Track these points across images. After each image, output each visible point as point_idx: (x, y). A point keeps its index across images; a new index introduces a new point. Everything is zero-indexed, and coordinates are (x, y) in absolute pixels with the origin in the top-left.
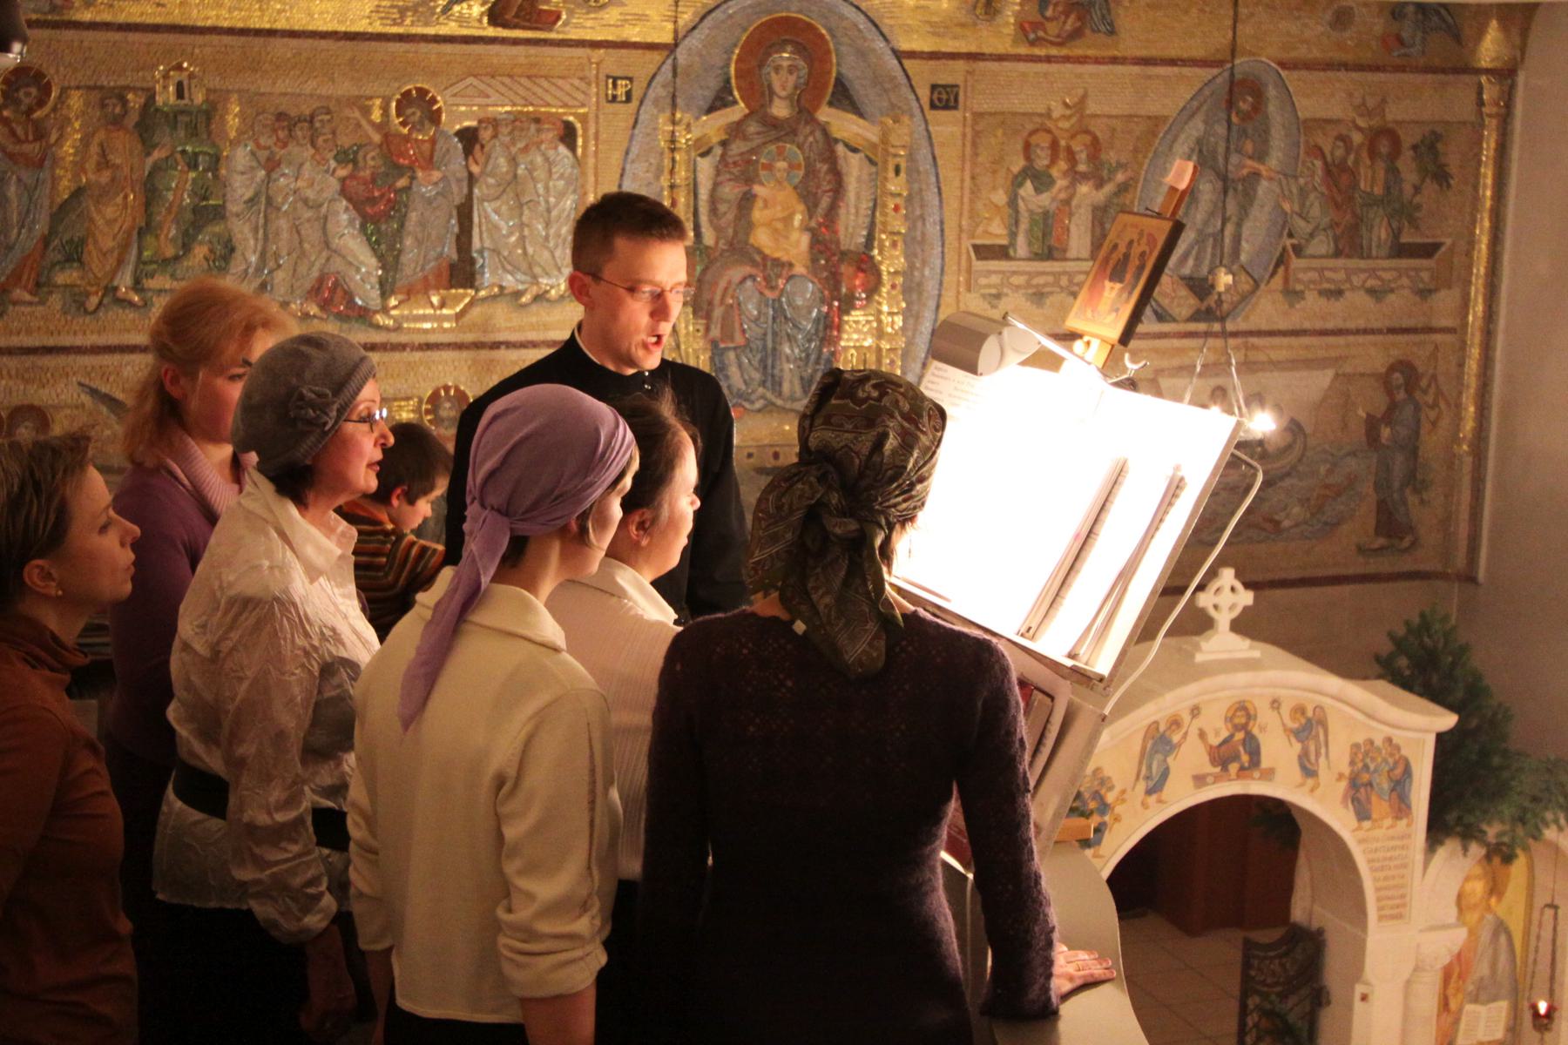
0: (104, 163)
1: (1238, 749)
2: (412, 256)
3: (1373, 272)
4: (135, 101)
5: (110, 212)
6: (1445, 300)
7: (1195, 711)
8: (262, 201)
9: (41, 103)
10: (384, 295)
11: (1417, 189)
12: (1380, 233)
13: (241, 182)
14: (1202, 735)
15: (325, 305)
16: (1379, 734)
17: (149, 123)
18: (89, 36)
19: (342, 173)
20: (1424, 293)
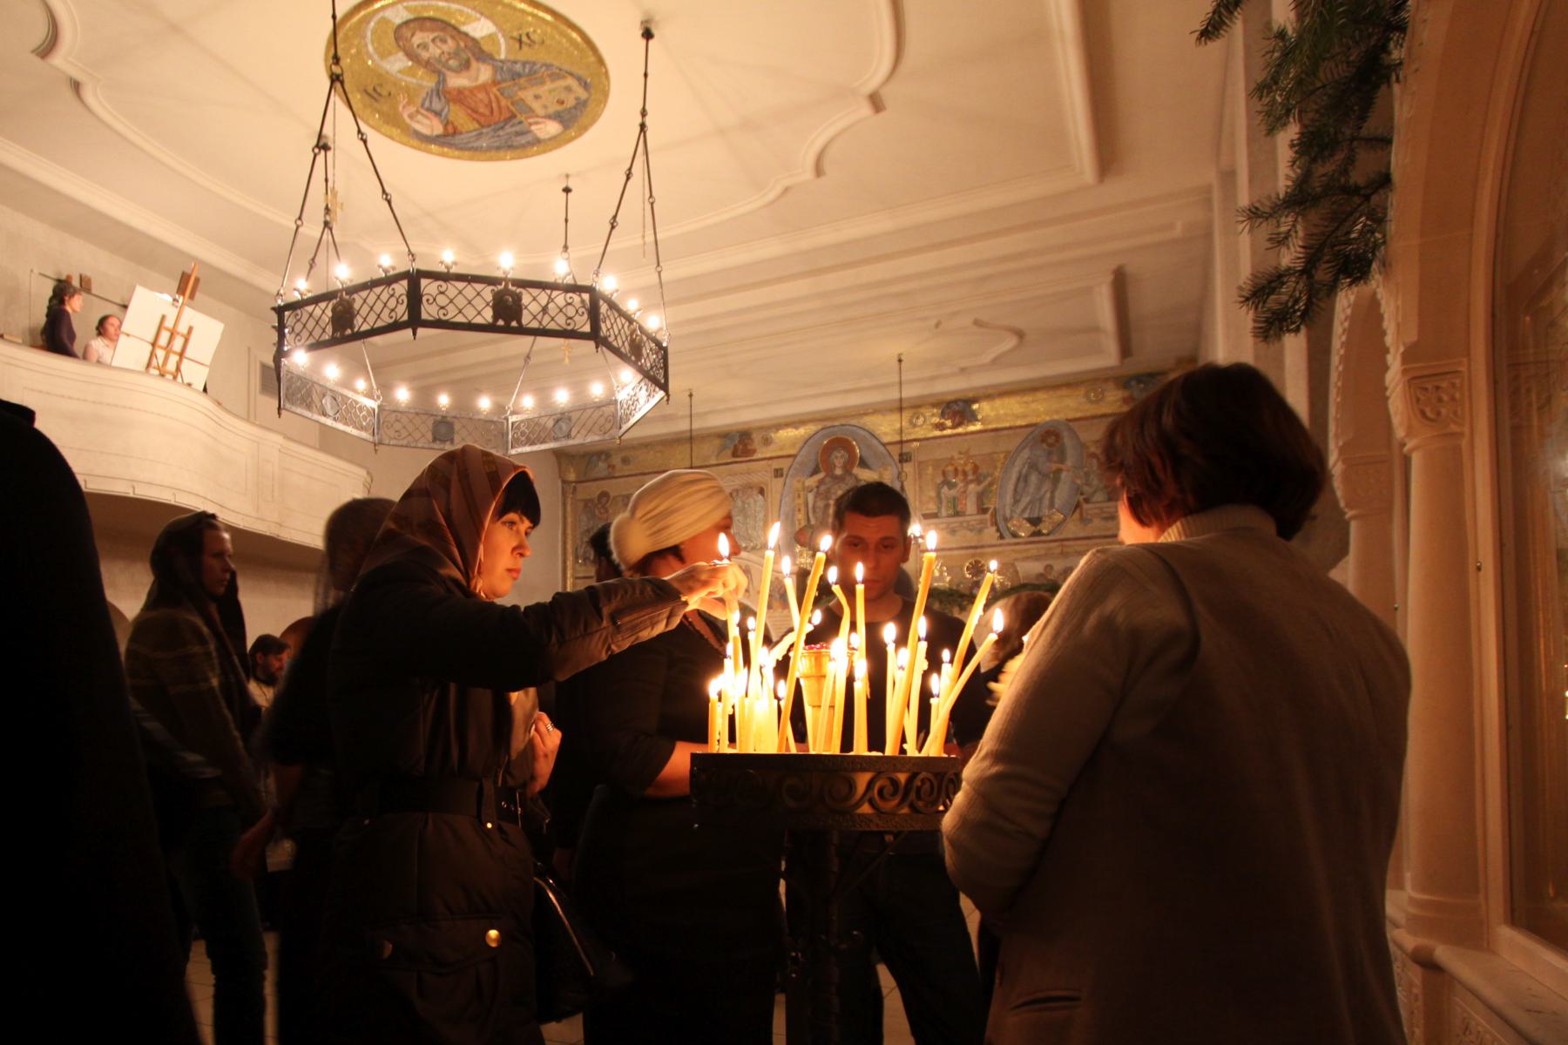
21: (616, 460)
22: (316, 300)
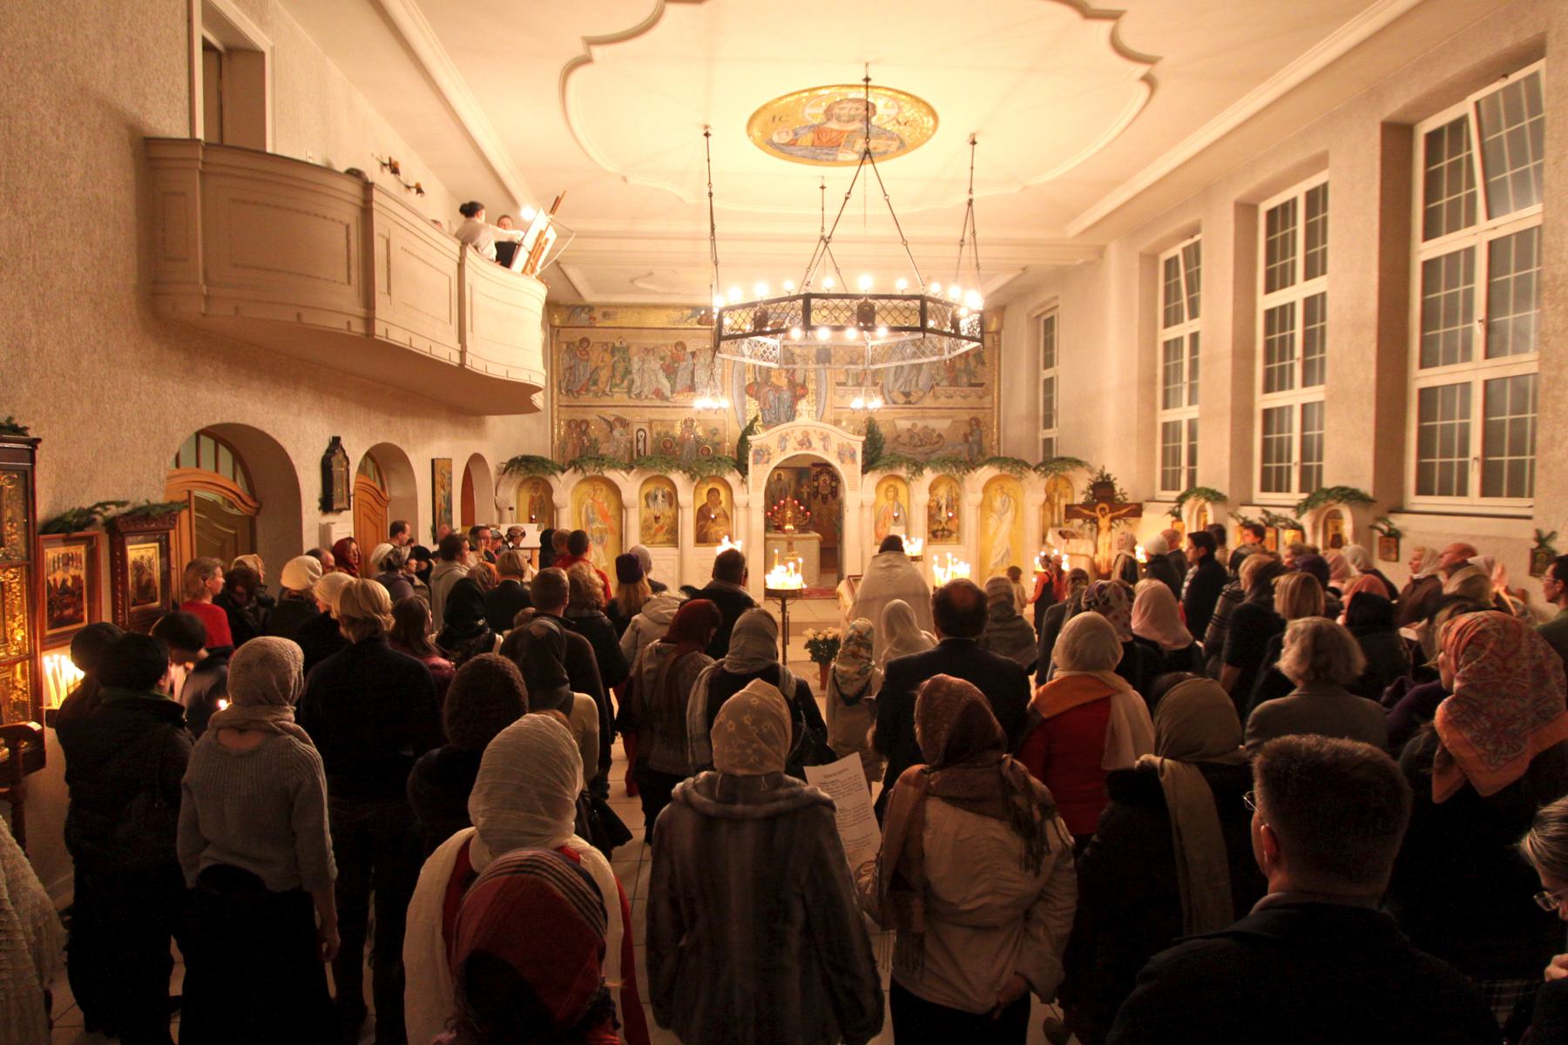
1: (805, 442)
2: (678, 387)
6: (987, 400)
12: (965, 380)
13: (636, 365)
17: (613, 351)
20: (839, 329)
21: (598, 314)
22: (743, 307)
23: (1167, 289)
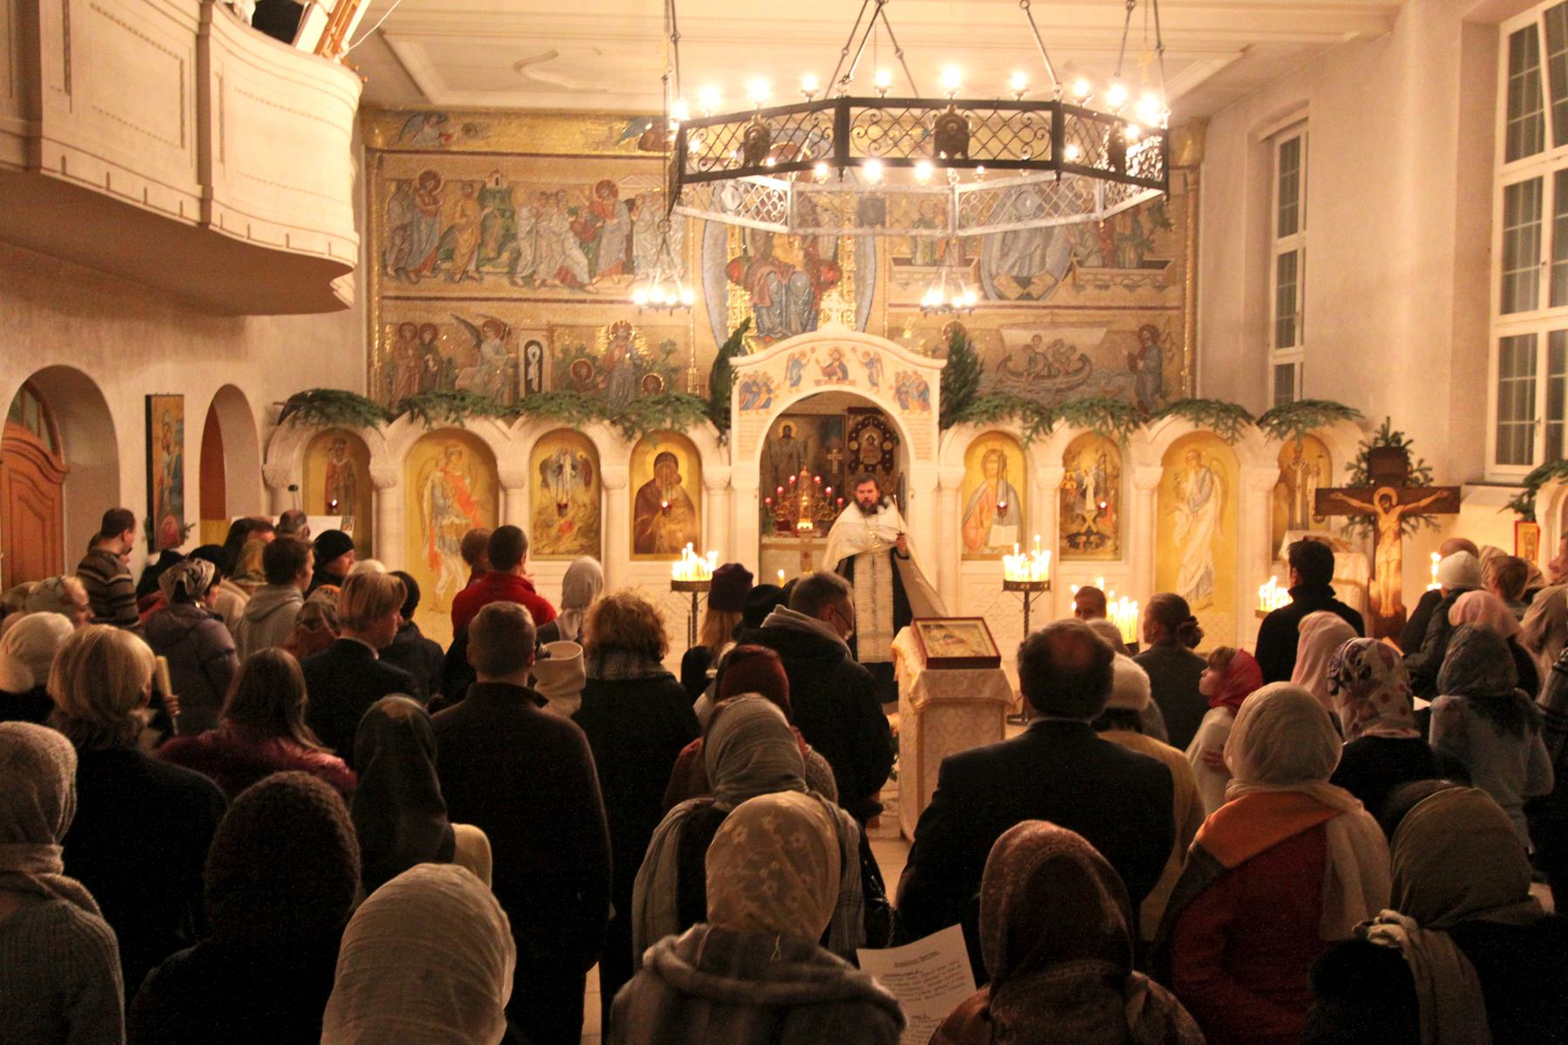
0: (463, 215)
1: (836, 369)
2: (603, 263)
3: (1127, 276)
4: (477, 187)
5: (466, 236)
7: (813, 350)
8: (534, 232)
9: (436, 187)
10: (591, 277)
11: (1152, 232)
12: (1130, 255)
14: (817, 361)
15: (563, 281)
16: (910, 369)
17: (483, 196)
18: (457, 157)
19: (572, 219)
20: (1161, 288)
21: (455, 129)
23: (1514, 87)
